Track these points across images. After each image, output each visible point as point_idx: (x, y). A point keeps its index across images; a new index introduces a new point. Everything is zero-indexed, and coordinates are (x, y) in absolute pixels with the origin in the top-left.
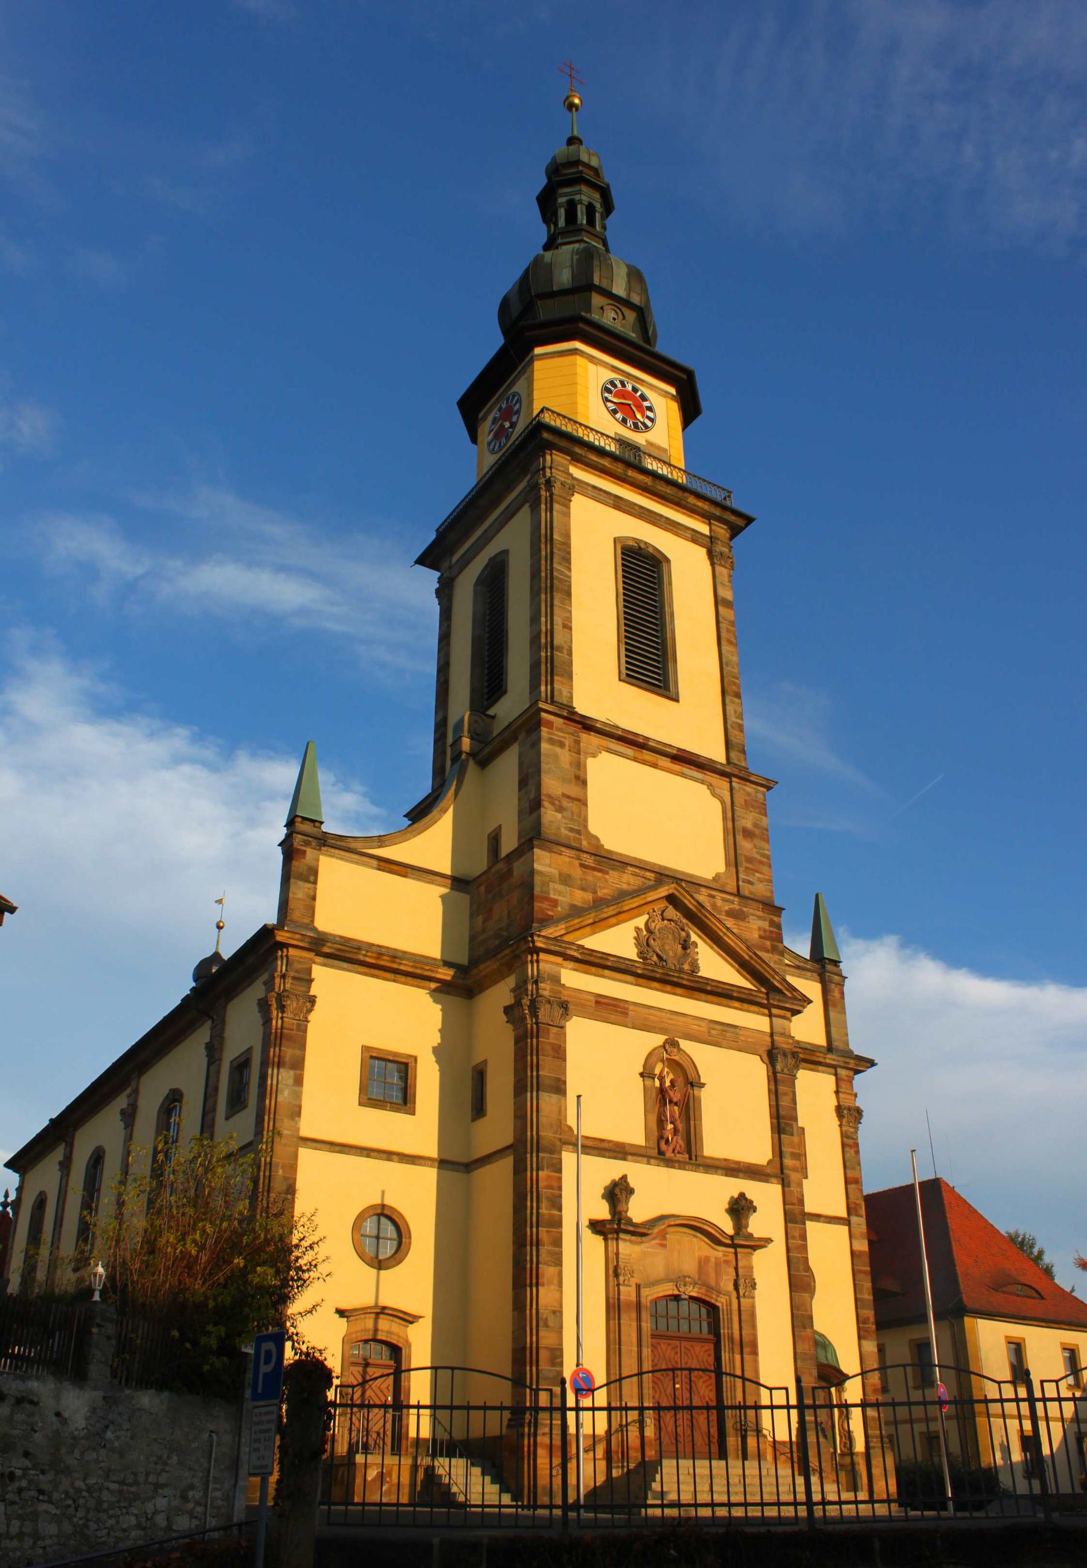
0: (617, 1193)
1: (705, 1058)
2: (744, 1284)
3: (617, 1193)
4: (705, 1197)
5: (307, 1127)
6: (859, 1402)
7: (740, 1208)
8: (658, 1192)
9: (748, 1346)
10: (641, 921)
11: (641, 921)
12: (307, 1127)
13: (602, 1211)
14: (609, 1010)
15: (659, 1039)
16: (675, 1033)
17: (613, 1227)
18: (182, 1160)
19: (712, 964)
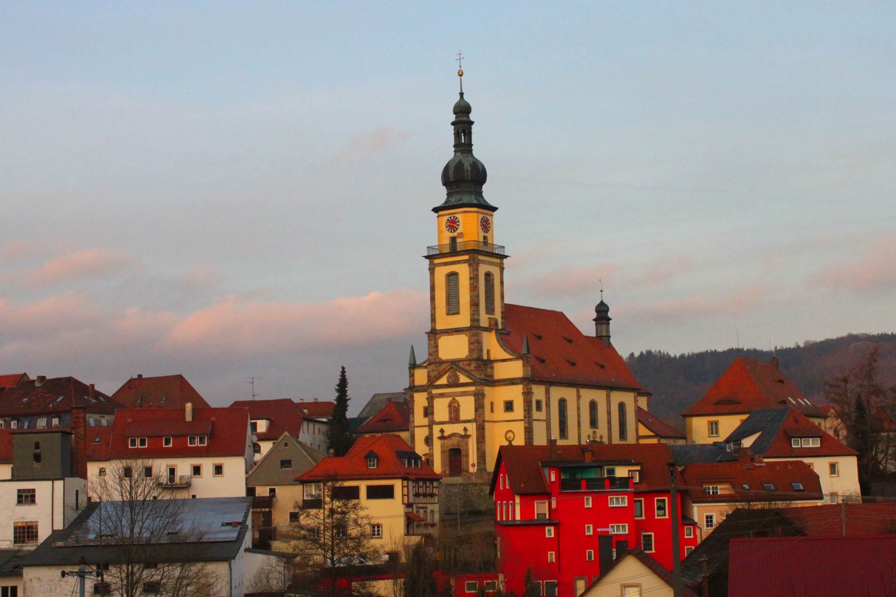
0: (442, 431)
1: (460, 399)
2: (467, 444)
3: (442, 431)
4: (458, 428)
5: (416, 424)
6: (495, 365)
7: (465, 429)
8: (449, 429)
9: (467, 456)
10: (745, 417)
11: (745, 417)
12: (416, 424)
13: (440, 435)
14: (441, 395)
15: (451, 399)
16: (453, 395)
17: (442, 438)
18: (116, 592)
19: (463, 379)
